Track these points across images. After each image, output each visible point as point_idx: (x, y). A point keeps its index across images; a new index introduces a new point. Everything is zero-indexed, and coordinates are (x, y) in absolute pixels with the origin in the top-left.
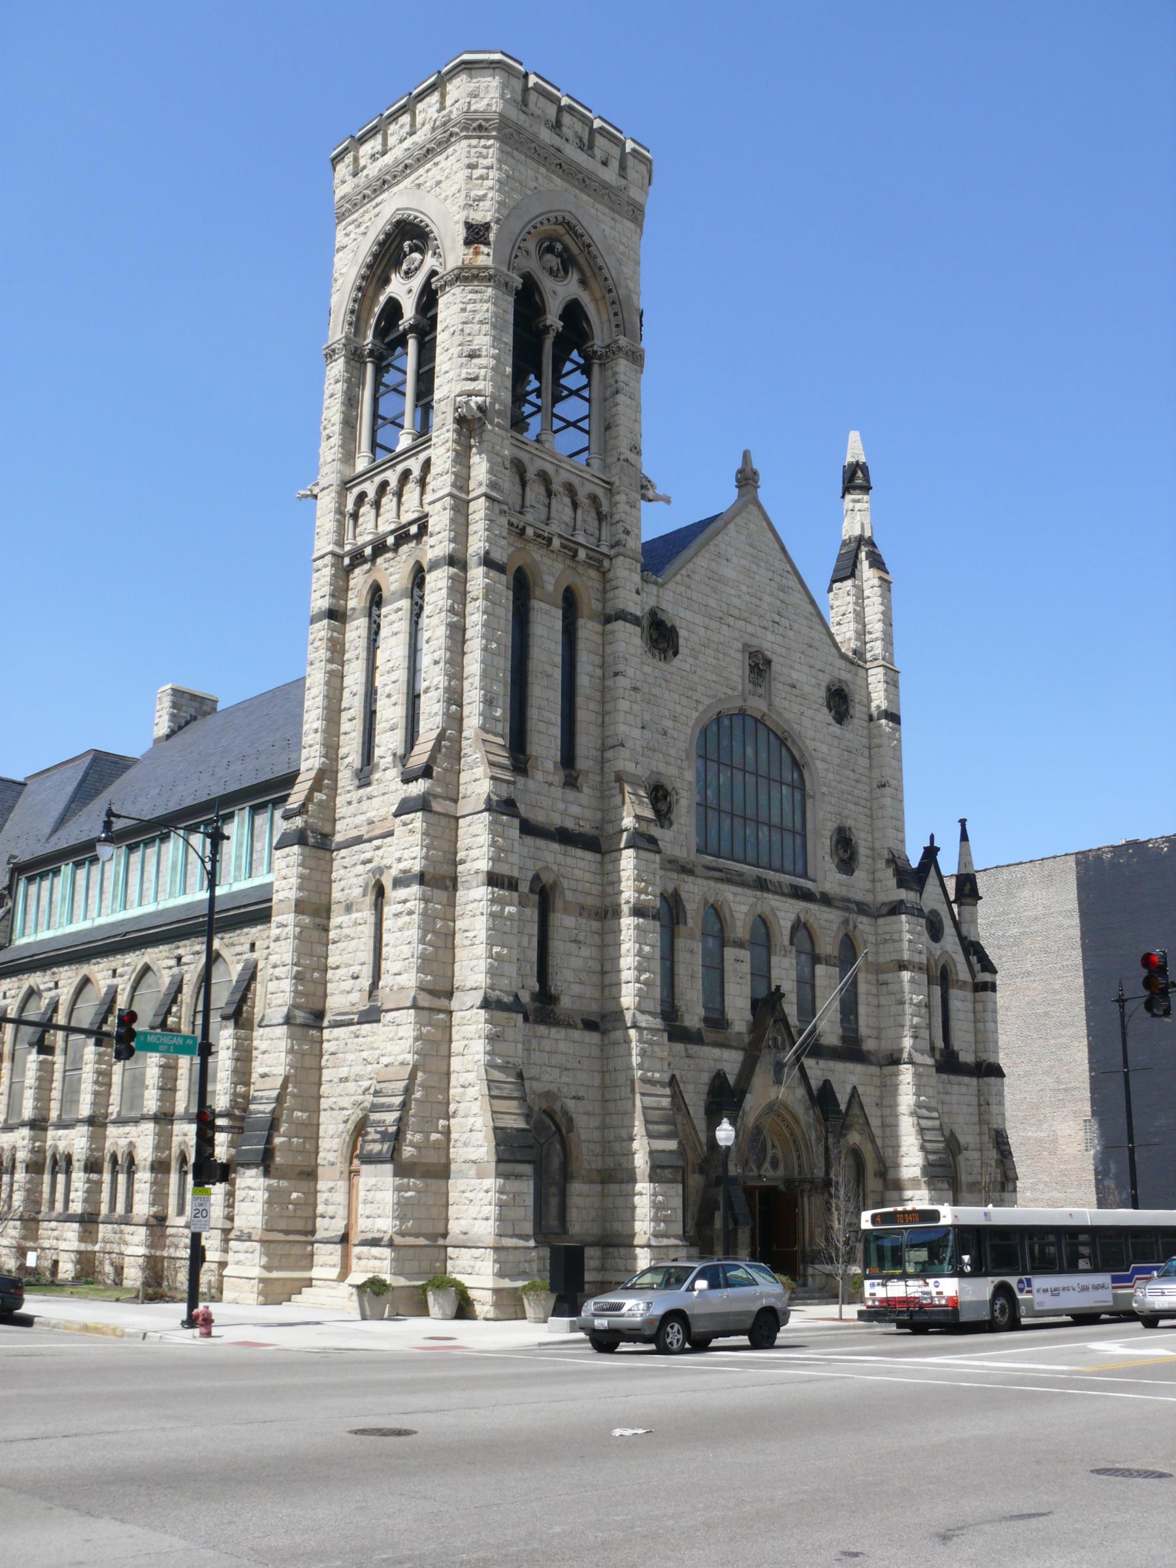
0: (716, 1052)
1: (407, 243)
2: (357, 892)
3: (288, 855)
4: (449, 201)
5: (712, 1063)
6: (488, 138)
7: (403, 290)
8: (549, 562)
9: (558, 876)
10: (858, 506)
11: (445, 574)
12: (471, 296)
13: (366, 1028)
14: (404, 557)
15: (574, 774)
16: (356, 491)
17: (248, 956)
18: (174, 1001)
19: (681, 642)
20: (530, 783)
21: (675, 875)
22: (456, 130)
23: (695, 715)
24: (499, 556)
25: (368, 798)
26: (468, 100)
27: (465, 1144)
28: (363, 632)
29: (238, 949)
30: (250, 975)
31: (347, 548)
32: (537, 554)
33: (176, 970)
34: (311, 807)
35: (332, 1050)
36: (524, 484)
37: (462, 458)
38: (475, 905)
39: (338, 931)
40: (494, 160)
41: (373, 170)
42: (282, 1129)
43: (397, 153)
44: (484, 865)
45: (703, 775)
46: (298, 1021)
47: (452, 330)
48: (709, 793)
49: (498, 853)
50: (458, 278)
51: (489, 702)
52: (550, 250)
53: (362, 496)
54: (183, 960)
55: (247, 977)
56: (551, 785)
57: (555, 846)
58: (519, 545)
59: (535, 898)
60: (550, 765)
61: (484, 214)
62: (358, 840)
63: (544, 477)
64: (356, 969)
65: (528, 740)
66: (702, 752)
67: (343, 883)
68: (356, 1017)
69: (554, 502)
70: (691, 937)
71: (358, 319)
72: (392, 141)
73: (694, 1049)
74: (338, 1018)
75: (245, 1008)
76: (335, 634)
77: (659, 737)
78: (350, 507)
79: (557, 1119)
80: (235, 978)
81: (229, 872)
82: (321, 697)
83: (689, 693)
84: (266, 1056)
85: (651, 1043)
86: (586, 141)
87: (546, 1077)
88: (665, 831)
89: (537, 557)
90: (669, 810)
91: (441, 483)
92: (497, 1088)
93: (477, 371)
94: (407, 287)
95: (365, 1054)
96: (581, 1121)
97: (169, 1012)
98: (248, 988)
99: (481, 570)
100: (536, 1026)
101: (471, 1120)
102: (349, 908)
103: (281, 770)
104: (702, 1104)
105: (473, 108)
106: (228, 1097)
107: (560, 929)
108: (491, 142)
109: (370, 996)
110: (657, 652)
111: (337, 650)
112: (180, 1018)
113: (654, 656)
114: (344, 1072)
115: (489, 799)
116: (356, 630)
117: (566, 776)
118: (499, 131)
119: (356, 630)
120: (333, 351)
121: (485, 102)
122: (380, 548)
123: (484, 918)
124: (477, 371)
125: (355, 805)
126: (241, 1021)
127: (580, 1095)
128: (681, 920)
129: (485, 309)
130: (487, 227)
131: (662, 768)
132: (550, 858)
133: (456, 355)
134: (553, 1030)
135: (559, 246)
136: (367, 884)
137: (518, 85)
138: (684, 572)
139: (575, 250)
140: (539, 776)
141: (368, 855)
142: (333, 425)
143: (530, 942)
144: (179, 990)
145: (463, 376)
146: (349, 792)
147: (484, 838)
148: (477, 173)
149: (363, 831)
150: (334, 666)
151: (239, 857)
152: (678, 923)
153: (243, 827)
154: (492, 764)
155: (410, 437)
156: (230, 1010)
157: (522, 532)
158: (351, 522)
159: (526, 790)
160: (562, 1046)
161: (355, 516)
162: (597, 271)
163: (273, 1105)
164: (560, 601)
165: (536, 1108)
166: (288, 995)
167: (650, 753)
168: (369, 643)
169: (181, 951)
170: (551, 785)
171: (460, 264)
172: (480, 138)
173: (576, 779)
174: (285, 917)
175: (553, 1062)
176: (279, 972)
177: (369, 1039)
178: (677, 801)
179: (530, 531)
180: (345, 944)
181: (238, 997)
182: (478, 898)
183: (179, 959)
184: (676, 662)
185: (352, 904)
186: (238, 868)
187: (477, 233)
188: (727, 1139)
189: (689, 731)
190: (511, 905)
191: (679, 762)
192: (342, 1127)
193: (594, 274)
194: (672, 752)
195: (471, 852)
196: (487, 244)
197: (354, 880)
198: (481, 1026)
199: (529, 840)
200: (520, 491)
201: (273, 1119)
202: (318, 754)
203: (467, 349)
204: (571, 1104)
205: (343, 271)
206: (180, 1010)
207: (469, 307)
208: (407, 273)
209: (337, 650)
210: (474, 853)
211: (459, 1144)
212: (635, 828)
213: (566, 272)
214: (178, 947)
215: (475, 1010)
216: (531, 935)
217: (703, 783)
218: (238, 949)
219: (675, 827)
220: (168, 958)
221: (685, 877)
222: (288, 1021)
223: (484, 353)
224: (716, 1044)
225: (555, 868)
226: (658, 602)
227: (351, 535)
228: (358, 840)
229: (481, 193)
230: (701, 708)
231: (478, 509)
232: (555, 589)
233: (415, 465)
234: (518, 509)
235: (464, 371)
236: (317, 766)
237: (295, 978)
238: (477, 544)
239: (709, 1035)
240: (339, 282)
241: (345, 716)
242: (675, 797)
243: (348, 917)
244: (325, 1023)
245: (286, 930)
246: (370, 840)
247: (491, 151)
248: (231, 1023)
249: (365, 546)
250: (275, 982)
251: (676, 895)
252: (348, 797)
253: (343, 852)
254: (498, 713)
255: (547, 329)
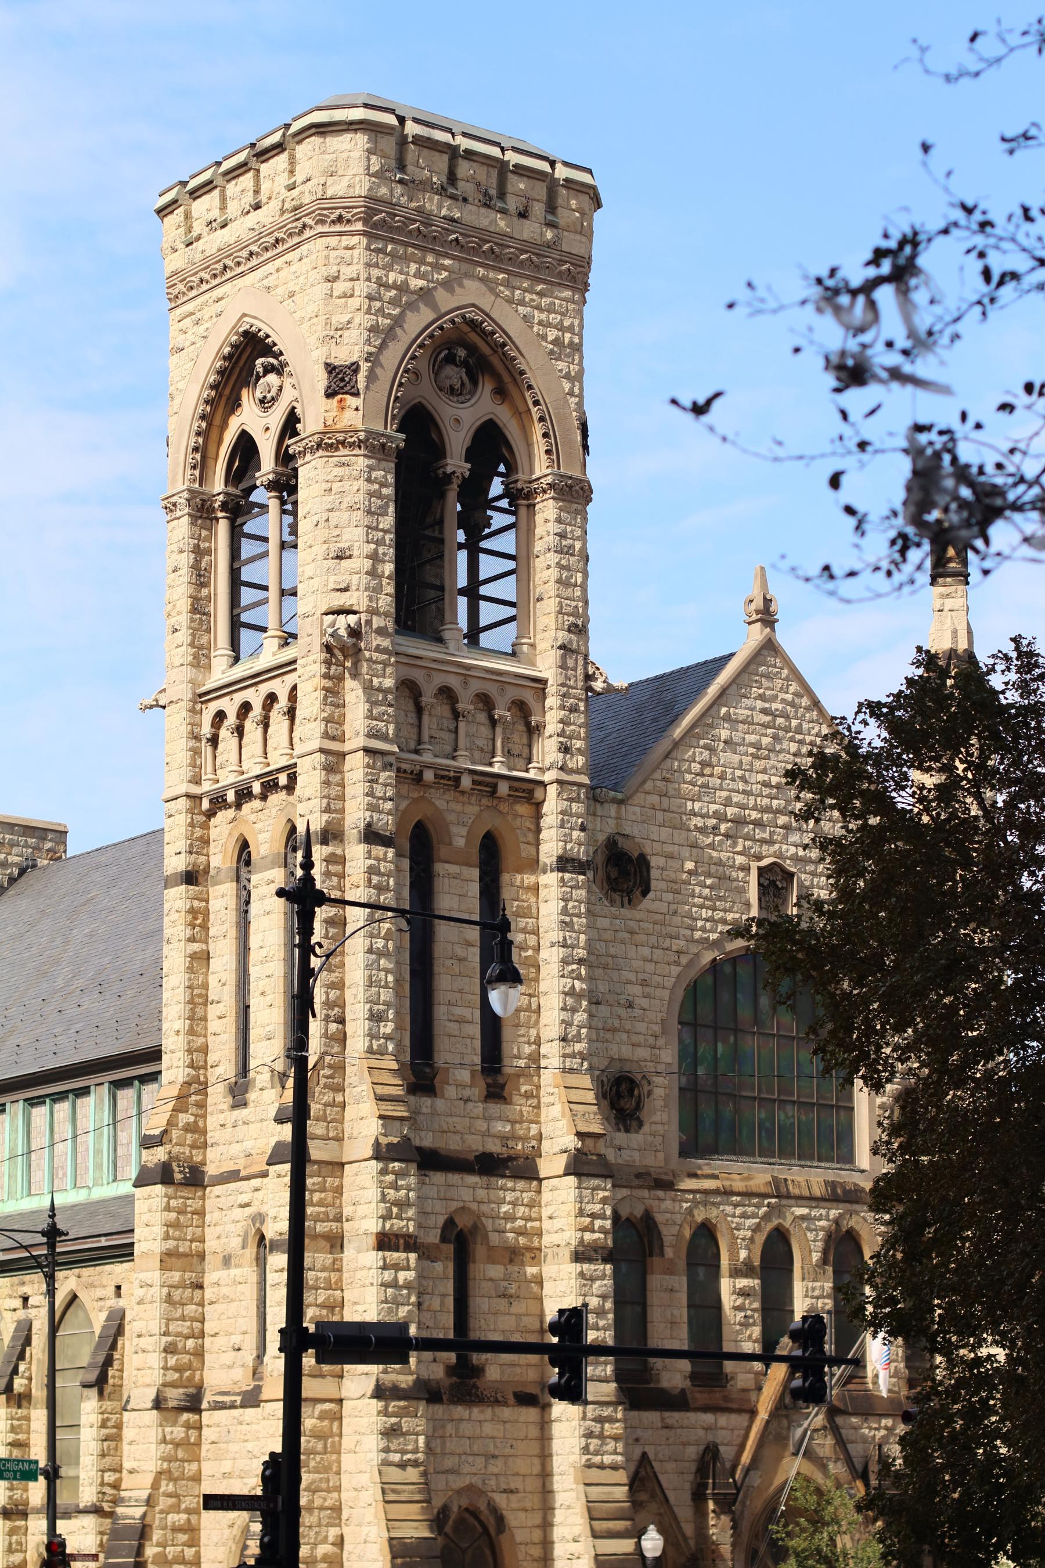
0: (708, 1418)
1: (259, 361)
2: (236, 1242)
3: (149, 1197)
4: (306, 325)
5: (701, 1433)
6: (352, 234)
7: (255, 419)
8: (458, 807)
9: (478, 1217)
10: (949, 603)
11: (319, 846)
12: (338, 471)
13: (250, 1412)
14: (274, 811)
15: (501, 1081)
16: (213, 707)
17: (112, 1302)
18: (21, 1357)
19: (654, 873)
20: (440, 1103)
21: (646, 1193)
22: (308, 221)
23: (675, 970)
24: (386, 822)
25: (244, 1123)
26: (322, 181)
27: (360, 1558)
28: (231, 902)
29: (99, 1293)
30: (116, 1327)
31: (206, 786)
32: (441, 801)
33: (21, 1314)
34: (175, 1134)
35: (213, 1438)
36: (419, 710)
37: (333, 694)
38: (365, 1272)
39: (216, 1289)
40: (361, 267)
41: (213, 242)
42: (155, 1538)
43: (241, 229)
44: (374, 1226)
45: (691, 1049)
46: (172, 1404)
47: (315, 518)
48: (701, 1071)
49: (393, 1208)
50: (319, 446)
51: (376, 1018)
52: (450, 359)
53: (221, 715)
54: (31, 1302)
55: (113, 1331)
56: (467, 1100)
57: (473, 1179)
58: (416, 795)
59: (449, 1249)
60: (464, 1076)
61: (351, 349)
62: (234, 1176)
63: (447, 693)
64: (236, 1339)
65: (436, 1048)
66: (689, 1017)
67: (219, 1229)
68: (238, 1399)
69: (462, 725)
70: (671, 1271)
71: (204, 458)
72: (233, 208)
73: (674, 1417)
74: (220, 1398)
75: (110, 1373)
76: (196, 903)
77: (622, 1012)
78: (206, 730)
79: (482, 1518)
80: (98, 1331)
81: (87, 1169)
82: (182, 989)
83: (667, 943)
84: (133, 1447)
85: (600, 1420)
86: (493, 192)
87: (466, 1469)
88: (632, 1136)
89: (441, 804)
90: (638, 1107)
91: (310, 733)
92: (394, 1491)
93: (349, 577)
94: (265, 421)
95: (250, 1446)
96: (514, 1519)
97: (15, 1371)
98: (113, 1346)
99: (361, 848)
100: (452, 1407)
101: (365, 1529)
102: (227, 1261)
103: (144, 1043)
104: (687, 1486)
105: (329, 194)
106: (94, 1489)
107: (484, 1284)
108: (355, 240)
109: (254, 1374)
110: (617, 897)
111: (199, 919)
112: (30, 1379)
113: (612, 902)
114: (227, 1466)
115: (377, 1144)
116: (222, 898)
117: (488, 1085)
118: (366, 221)
119: (222, 898)
120: (174, 505)
121: (345, 182)
122: (244, 795)
123: (374, 1289)
124: (349, 577)
125: (229, 1129)
126: (108, 1389)
127: (513, 1486)
128: (656, 1250)
129: (356, 490)
130: (355, 368)
131: (626, 1051)
132: (466, 1195)
133: (320, 557)
134: (476, 1410)
135: (462, 353)
136: (246, 1233)
137: (389, 145)
138: (657, 775)
139: (486, 350)
140: (451, 1092)
141: (244, 1198)
142: (179, 613)
143: (442, 1304)
144: (28, 1341)
145: (332, 586)
146: (222, 1112)
147: (372, 1193)
148: (340, 287)
149: (240, 1164)
150: (196, 947)
151: (98, 1152)
152: (651, 1255)
153: (102, 1109)
154: (380, 1098)
155: (276, 641)
156: (92, 1376)
157: (418, 778)
158: (209, 749)
159: (434, 1113)
160: (488, 1429)
161: (214, 741)
162: (517, 376)
163: (144, 1509)
164: (475, 857)
165: (455, 1509)
166: (156, 1372)
167: (609, 1036)
168: (239, 916)
169: (27, 1290)
170: (467, 1100)
171: (320, 427)
172: (341, 234)
173: (503, 1087)
174: (149, 1274)
175: (475, 1448)
176: (144, 1342)
177: (254, 1427)
178: (650, 1093)
179: (429, 776)
180: (224, 1306)
181: (101, 1359)
182: (368, 1265)
183: (26, 1299)
184: (647, 903)
185: (230, 1256)
186: (98, 1167)
187: (342, 380)
188: (654, 1549)
189: (666, 994)
190: (408, 1269)
191: (651, 1040)
192: (227, 1532)
193: (515, 380)
194: (641, 1027)
195: (359, 1208)
196: (356, 394)
197: (231, 1227)
198: (374, 1419)
199: (438, 1178)
200: (415, 721)
201: (144, 1526)
202: (181, 1063)
203: (334, 548)
204: (500, 1500)
205: (181, 385)
206: (29, 1369)
207: (336, 486)
208: (262, 401)
209: (199, 919)
210: (362, 1210)
211: (353, 1557)
212: (577, 1150)
213: (475, 382)
214: (23, 1283)
215: (367, 1401)
216: (443, 1296)
217: (689, 1058)
218: (99, 1293)
219: (646, 1128)
220: (10, 1297)
221: (660, 1193)
222: (158, 1404)
223: (356, 553)
224: (705, 1409)
225: (474, 1206)
226: (618, 825)
227: (210, 769)
228: (234, 1176)
229: (346, 318)
230: (684, 960)
231: (356, 766)
232: (467, 843)
233: (280, 687)
234: (412, 745)
235: (332, 578)
236: (181, 1080)
237: (165, 1351)
238: (355, 815)
239: (701, 1397)
240: (177, 401)
241: (213, 1011)
242: (646, 1088)
243: (226, 1272)
244: (204, 1405)
245: (152, 1291)
246: (248, 1178)
247: (356, 252)
248: (94, 1392)
249: (226, 788)
250: (141, 1355)
251: (648, 1218)
252: (221, 1118)
253: (218, 1190)
254: (388, 1028)
255: (448, 478)
